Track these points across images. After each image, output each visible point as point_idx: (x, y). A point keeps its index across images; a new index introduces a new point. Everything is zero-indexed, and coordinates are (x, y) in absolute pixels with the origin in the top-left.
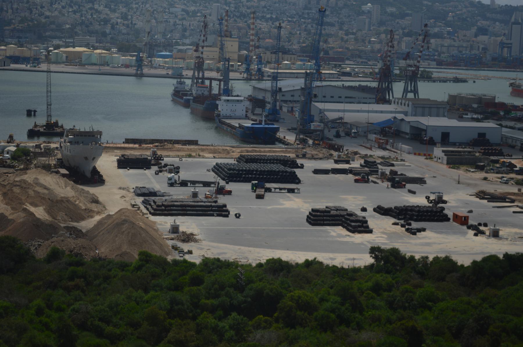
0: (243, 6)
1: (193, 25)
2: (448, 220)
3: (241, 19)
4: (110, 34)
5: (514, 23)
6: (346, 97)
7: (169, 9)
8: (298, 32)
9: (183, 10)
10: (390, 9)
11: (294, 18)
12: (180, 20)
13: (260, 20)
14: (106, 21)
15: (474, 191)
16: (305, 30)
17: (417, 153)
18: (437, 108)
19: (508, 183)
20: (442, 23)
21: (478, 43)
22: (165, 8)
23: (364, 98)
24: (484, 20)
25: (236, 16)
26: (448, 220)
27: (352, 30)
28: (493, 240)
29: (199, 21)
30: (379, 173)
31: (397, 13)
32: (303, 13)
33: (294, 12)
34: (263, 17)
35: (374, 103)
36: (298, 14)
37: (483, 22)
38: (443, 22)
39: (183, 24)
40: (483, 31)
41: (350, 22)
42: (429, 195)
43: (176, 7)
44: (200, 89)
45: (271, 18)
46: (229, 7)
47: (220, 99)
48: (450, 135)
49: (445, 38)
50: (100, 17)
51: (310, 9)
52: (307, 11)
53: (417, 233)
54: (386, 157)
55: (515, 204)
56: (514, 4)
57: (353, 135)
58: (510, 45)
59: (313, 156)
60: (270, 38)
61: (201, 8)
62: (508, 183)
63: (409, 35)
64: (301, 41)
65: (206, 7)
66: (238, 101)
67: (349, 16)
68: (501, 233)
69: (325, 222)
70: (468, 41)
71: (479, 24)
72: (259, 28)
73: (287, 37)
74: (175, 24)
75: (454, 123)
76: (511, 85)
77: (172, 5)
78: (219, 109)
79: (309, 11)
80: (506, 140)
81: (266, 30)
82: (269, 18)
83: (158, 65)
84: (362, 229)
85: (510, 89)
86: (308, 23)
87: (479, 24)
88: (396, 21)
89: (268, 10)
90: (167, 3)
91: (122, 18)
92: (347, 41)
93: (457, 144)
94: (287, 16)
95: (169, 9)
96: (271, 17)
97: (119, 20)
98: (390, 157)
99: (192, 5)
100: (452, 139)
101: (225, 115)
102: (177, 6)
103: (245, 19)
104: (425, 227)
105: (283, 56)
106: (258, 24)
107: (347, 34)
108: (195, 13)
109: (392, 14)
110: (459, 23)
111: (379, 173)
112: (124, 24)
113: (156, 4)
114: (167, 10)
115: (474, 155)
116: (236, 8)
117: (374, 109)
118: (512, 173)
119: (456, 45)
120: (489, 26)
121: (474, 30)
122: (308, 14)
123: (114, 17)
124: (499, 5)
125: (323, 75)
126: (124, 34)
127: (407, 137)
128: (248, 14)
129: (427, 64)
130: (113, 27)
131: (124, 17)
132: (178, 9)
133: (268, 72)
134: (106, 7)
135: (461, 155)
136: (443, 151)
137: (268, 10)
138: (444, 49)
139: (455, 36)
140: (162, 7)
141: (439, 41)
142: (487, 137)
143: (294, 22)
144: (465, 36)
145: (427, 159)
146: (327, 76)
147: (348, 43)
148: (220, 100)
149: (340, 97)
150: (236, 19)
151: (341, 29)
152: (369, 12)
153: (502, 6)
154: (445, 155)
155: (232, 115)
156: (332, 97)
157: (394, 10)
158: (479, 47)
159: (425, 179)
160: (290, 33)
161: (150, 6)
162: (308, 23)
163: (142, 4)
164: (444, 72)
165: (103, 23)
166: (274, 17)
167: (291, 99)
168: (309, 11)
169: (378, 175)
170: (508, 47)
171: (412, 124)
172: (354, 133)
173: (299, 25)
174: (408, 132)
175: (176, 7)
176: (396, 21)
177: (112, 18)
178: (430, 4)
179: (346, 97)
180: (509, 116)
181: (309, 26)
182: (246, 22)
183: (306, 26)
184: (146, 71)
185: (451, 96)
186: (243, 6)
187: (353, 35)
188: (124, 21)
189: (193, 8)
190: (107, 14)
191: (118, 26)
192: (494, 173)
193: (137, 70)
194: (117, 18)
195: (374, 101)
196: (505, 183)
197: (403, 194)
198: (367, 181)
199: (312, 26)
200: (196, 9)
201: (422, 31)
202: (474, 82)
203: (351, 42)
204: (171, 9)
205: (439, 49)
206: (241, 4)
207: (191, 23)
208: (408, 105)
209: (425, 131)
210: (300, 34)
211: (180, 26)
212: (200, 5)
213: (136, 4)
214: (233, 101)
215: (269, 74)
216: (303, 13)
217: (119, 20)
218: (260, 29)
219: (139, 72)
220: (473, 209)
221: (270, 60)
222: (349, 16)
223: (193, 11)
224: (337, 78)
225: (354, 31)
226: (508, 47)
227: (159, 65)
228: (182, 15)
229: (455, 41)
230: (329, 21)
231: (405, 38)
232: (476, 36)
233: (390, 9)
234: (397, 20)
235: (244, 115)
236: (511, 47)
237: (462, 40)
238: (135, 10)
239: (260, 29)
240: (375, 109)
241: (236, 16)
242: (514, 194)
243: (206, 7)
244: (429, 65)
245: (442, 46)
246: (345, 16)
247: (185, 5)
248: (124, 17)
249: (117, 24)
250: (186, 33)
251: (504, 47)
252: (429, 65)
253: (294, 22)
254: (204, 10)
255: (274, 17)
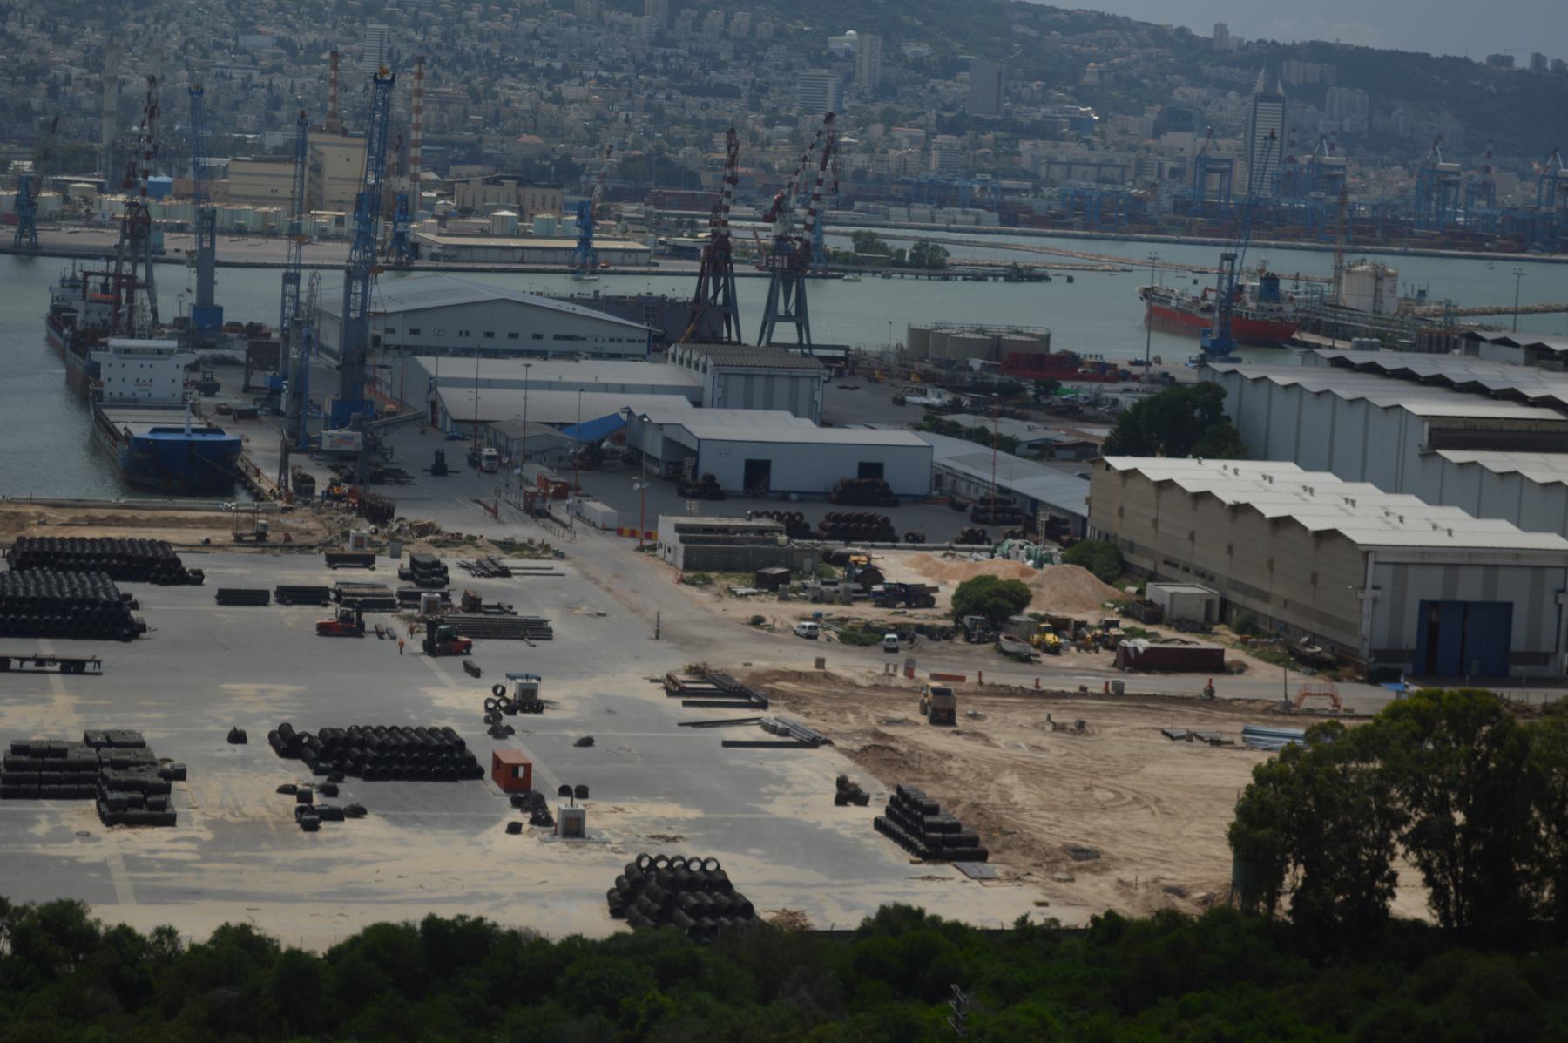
0: (468, 31)
1: (303, 86)
2: (477, 773)
3: (455, 73)
4: (44, 112)
5: (1263, 97)
6: (557, 337)
7: (236, 39)
8: (623, 115)
9: (280, 42)
10: (912, 49)
11: (620, 70)
12: (263, 72)
13: (514, 75)
14: (33, 73)
15: (677, 663)
16: (647, 109)
17: (627, 529)
18: (792, 377)
19: (815, 637)
20: (1065, 91)
21: (1161, 154)
22: (225, 35)
23: (612, 340)
24: (1193, 85)
25: (441, 63)
26: (477, 773)
27: (789, 110)
28: (560, 848)
29: (321, 78)
30: (422, 603)
31: (935, 58)
32: (650, 57)
33: (624, 53)
34: (524, 66)
35: (643, 358)
36: (633, 57)
37: (1189, 91)
38: (1070, 88)
39: (270, 84)
40: (1179, 119)
41: (790, 84)
42: (503, 681)
43: (259, 33)
44: (97, 306)
45: (548, 72)
46: (425, 33)
47: (105, 344)
48: (773, 467)
49: (1063, 138)
50: (17, 61)
51: (673, 43)
52: (661, 50)
53: (323, 824)
54: (518, 541)
55: (768, 715)
56: (1285, 39)
57: (484, 464)
58: (1225, 166)
59: (288, 538)
60: (535, 130)
61: (337, 36)
62: (815, 637)
63: (952, 127)
64: (629, 140)
65: (352, 33)
66: (159, 351)
67: (789, 67)
68: (590, 823)
69: (46, 787)
70: (1133, 149)
71: (1176, 96)
72: (502, 99)
73: (586, 127)
74: (247, 85)
75: (803, 430)
76: (1147, 294)
77: (247, 27)
78: (102, 378)
79: (669, 51)
80: (954, 482)
81: (526, 106)
82: (541, 70)
83: (107, 218)
84: (145, 811)
85: (1142, 308)
86: (658, 88)
87: (1176, 96)
88: (929, 86)
89: (544, 44)
90: (232, 20)
91: (85, 65)
92: (768, 143)
93: (794, 497)
94: (601, 63)
95: (236, 39)
96: (549, 65)
97: (75, 71)
98: (531, 542)
99: (311, 27)
100: (778, 480)
101: (116, 394)
102: (263, 29)
103: (467, 73)
104: (363, 805)
105: (521, 190)
106: (504, 86)
107: (769, 124)
108: (314, 49)
109: (918, 64)
110: (1116, 94)
111: (422, 603)
112: (88, 83)
113: (198, 23)
114: (230, 41)
115: (774, 541)
116: (444, 37)
117: (601, 380)
118: (864, 599)
119: (1093, 161)
120: (1206, 104)
121: (1152, 114)
122: (665, 58)
123: (65, 61)
124: (1241, 41)
125: (601, 256)
126: (85, 113)
127: (657, 470)
128: (478, 57)
129: (971, 218)
130: (53, 90)
131: (93, 60)
132: (263, 41)
133: (431, 244)
134: (42, 27)
135: (731, 542)
136: (680, 528)
137: (544, 44)
138: (1057, 173)
139: (1095, 134)
140: (215, 30)
141: (1044, 147)
142: (889, 476)
143: (616, 85)
144: (1124, 132)
145: (641, 549)
146: (616, 257)
147: (771, 149)
148: (107, 350)
149: (539, 337)
150: (440, 71)
151: (754, 106)
152: (849, 55)
153: (1249, 43)
154: (682, 540)
155: (139, 394)
156: (513, 336)
157: (924, 49)
158: (1161, 166)
159: (550, 624)
160: (599, 117)
161: (181, 27)
162: (658, 88)
163: (157, 21)
164: (1017, 248)
165: (23, 78)
166: (558, 65)
167: (411, 340)
168: (669, 51)
169: (417, 607)
170: (1222, 172)
171: (668, 433)
172: (489, 458)
173: (630, 94)
174: (659, 455)
175: (259, 33)
176: (929, 86)
177: (53, 64)
178: (1033, 33)
179: (557, 337)
180: (1056, 400)
181: (661, 95)
182: (467, 81)
183: (650, 97)
184: (46, 236)
185: (919, 336)
186: (468, 31)
187: (788, 124)
188: (91, 72)
189: (310, 37)
190: (40, 52)
191: (69, 89)
192: (805, 599)
193: (20, 234)
194: (72, 63)
195: (643, 348)
196: (808, 637)
197: (444, 677)
198: (358, 631)
199: (669, 98)
200: (321, 39)
201: (820, 133)
202: (1070, 280)
203: (782, 148)
204: (241, 38)
205: (1043, 172)
206: (462, 27)
207: (298, 82)
208: (705, 369)
209: (695, 454)
210: (627, 120)
211: (264, 91)
212: (334, 26)
213: (136, 21)
214: (138, 351)
215: (435, 250)
216: (650, 57)
217: (75, 71)
218: (507, 103)
219: (24, 240)
220: (592, 733)
221: (468, 204)
222: (789, 67)
223: (309, 46)
224: (650, 264)
225: (793, 114)
226: (1222, 172)
227: (113, 218)
228: (275, 56)
229: (1092, 148)
230: (727, 81)
231: (940, 138)
232: (1157, 132)
233: (912, 49)
234: (933, 82)
235: (179, 396)
236: (1229, 171)
237: (1115, 144)
238: (130, 39)
239: (507, 103)
240: (606, 379)
241: (441, 63)
242: (799, 676)
243: (352, 33)
244: (978, 222)
245: (1051, 161)
246: (777, 67)
247: (289, 25)
248: (93, 60)
249: (68, 81)
250: (277, 113)
251: (1211, 171)
252: (978, 222)
253: (616, 85)
254: (345, 43)
255: (558, 65)
